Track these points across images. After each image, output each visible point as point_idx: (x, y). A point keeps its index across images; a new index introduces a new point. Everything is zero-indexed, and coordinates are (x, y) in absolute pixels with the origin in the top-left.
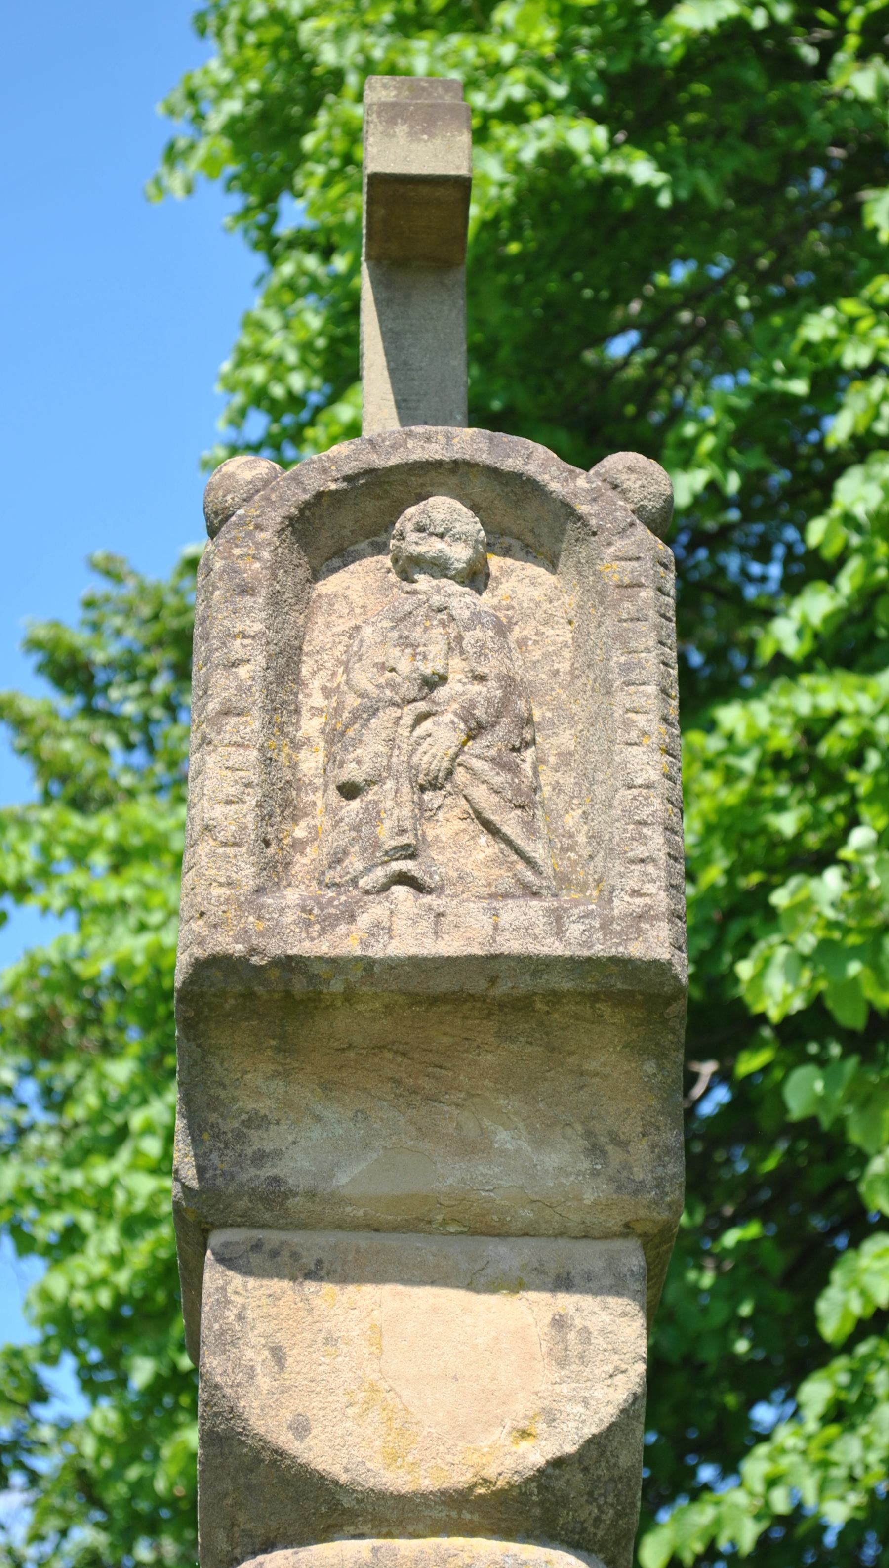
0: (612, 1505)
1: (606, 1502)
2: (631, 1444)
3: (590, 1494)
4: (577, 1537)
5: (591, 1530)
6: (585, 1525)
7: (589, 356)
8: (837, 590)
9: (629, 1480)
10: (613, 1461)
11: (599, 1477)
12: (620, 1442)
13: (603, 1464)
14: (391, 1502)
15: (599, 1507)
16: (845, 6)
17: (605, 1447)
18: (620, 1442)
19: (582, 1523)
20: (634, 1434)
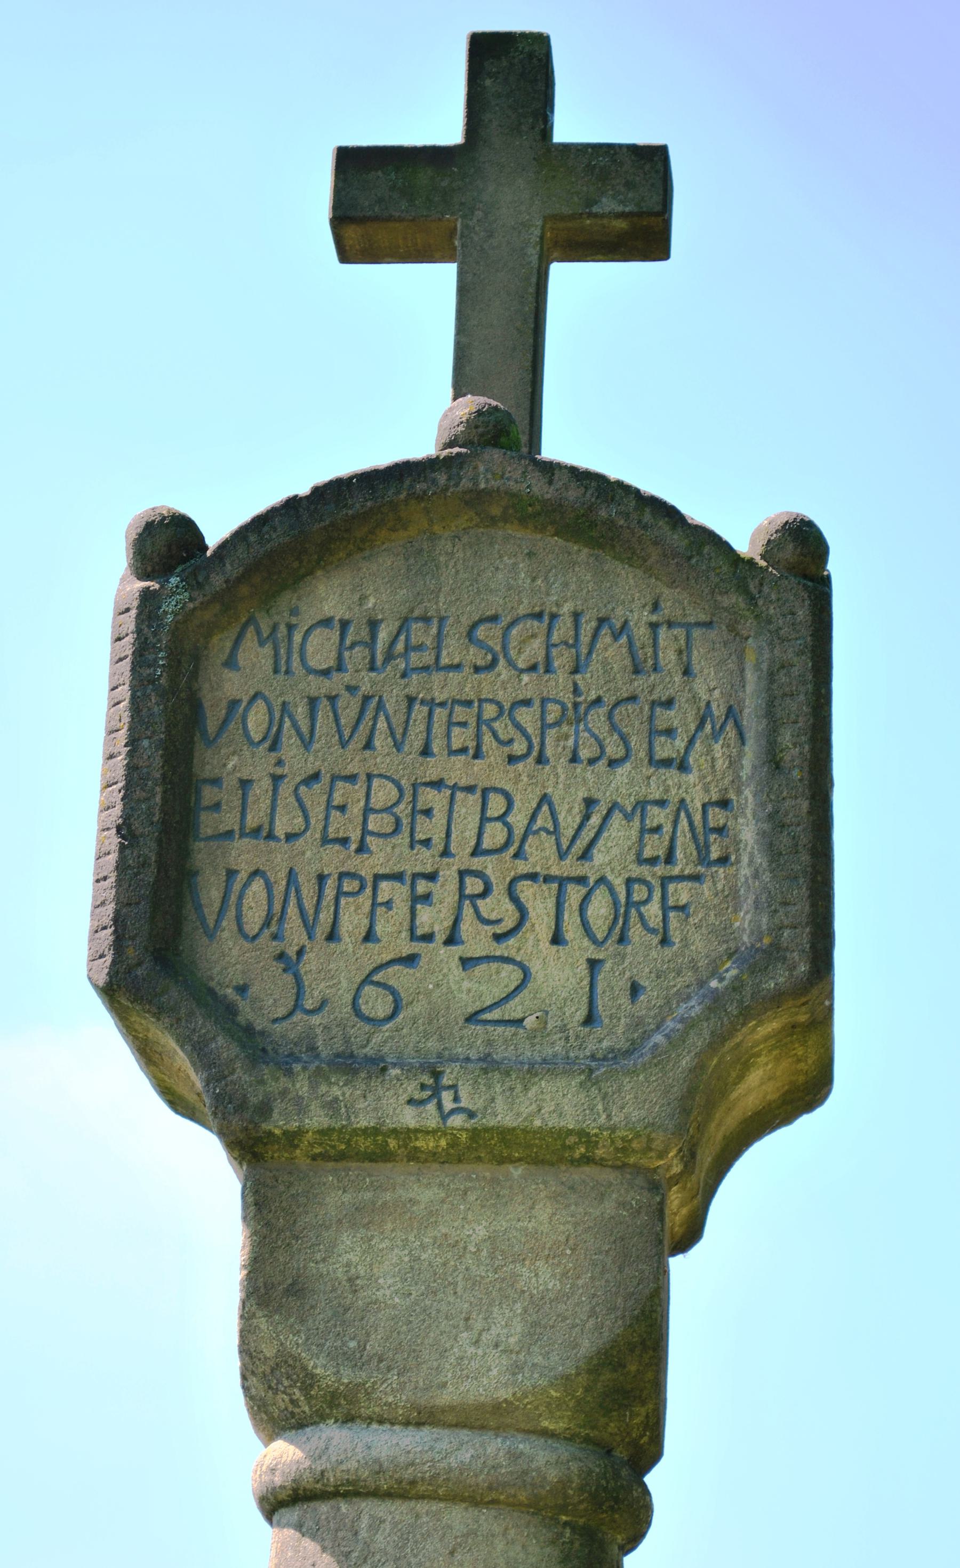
0: (291, 1386)
1: (286, 1387)
2: (263, 1337)
3: (270, 1387)
4: (293, 1420)
5: (297, 1410)
6: (290, 1410)
7: (209, 553)
8: (632, 681)
9: (286, 1362)
10: (261, 1356)
11: (264, 1373)
12: (254, 1341)
13: (258, 1363)
14: (827, 1003)
15: (284, 1392)
16: (501, 1562)
17: (249, 1349)
18: (254, 1341)
19: (286, 1409)
20: (259, 1328)
